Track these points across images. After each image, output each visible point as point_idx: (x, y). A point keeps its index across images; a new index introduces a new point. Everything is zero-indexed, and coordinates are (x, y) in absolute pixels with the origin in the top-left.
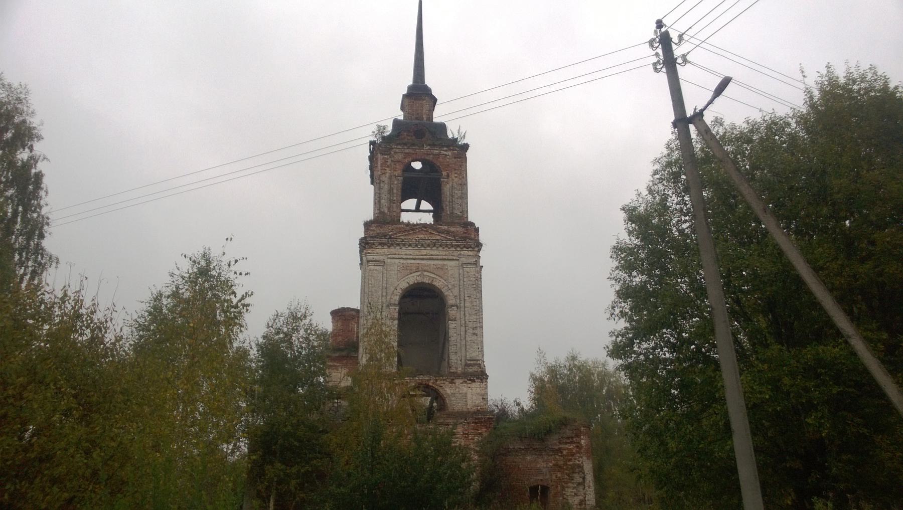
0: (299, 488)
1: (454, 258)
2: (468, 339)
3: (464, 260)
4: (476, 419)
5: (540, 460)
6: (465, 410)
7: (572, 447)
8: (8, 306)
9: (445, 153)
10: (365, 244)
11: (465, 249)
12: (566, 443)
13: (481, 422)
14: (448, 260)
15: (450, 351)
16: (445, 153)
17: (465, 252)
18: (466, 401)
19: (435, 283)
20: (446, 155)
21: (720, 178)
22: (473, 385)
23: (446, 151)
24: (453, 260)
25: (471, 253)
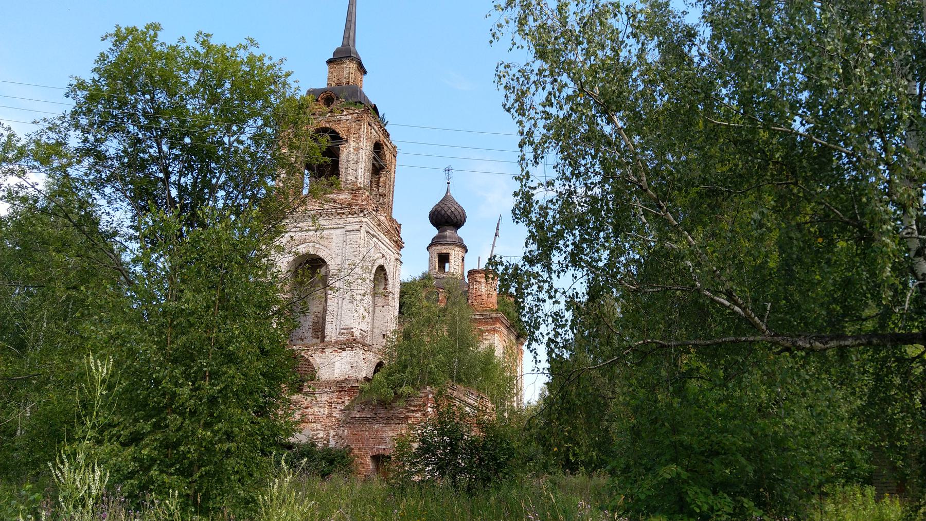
0: (880, 332)
1: (340, 226)
2: (344, 307)
3: (349, 228)
4: (340, 387)
5: (387, 429)
6: (332, 379)
7: (418, 415)
8: (403, 285)
9: (345, 117)
10: (465, 221)
11: (350, 216)
12: (413, 411)
13: (345, 391)
14: (334, 228)
15: (327, 320)
16: (345, 117)
17: (351, 219)
18: (334, 370)
19: (318, 254)
20: (347, 120)
21: (866, 113)
22: (344, 353)
23: (346, 115)
24: (338, 228)
25: (356, 220)
